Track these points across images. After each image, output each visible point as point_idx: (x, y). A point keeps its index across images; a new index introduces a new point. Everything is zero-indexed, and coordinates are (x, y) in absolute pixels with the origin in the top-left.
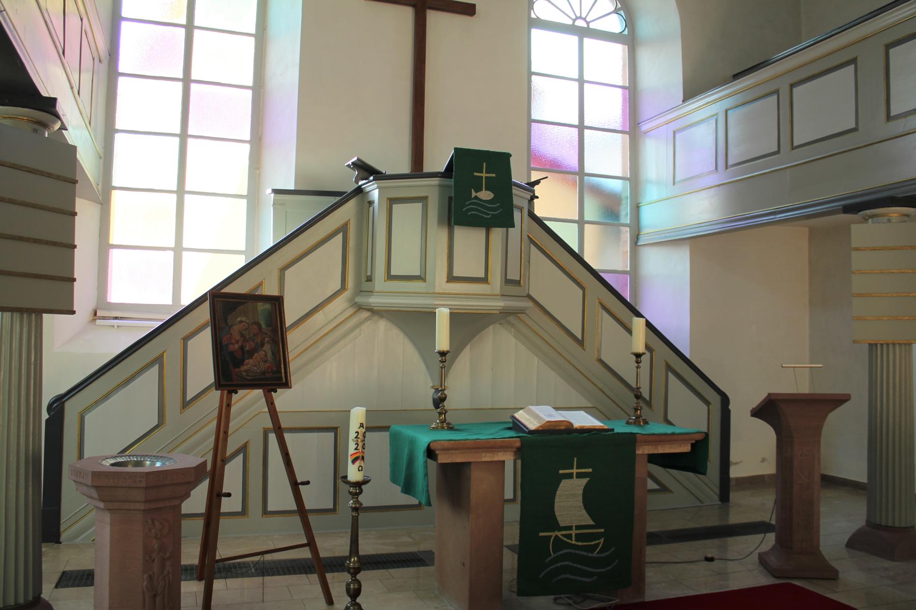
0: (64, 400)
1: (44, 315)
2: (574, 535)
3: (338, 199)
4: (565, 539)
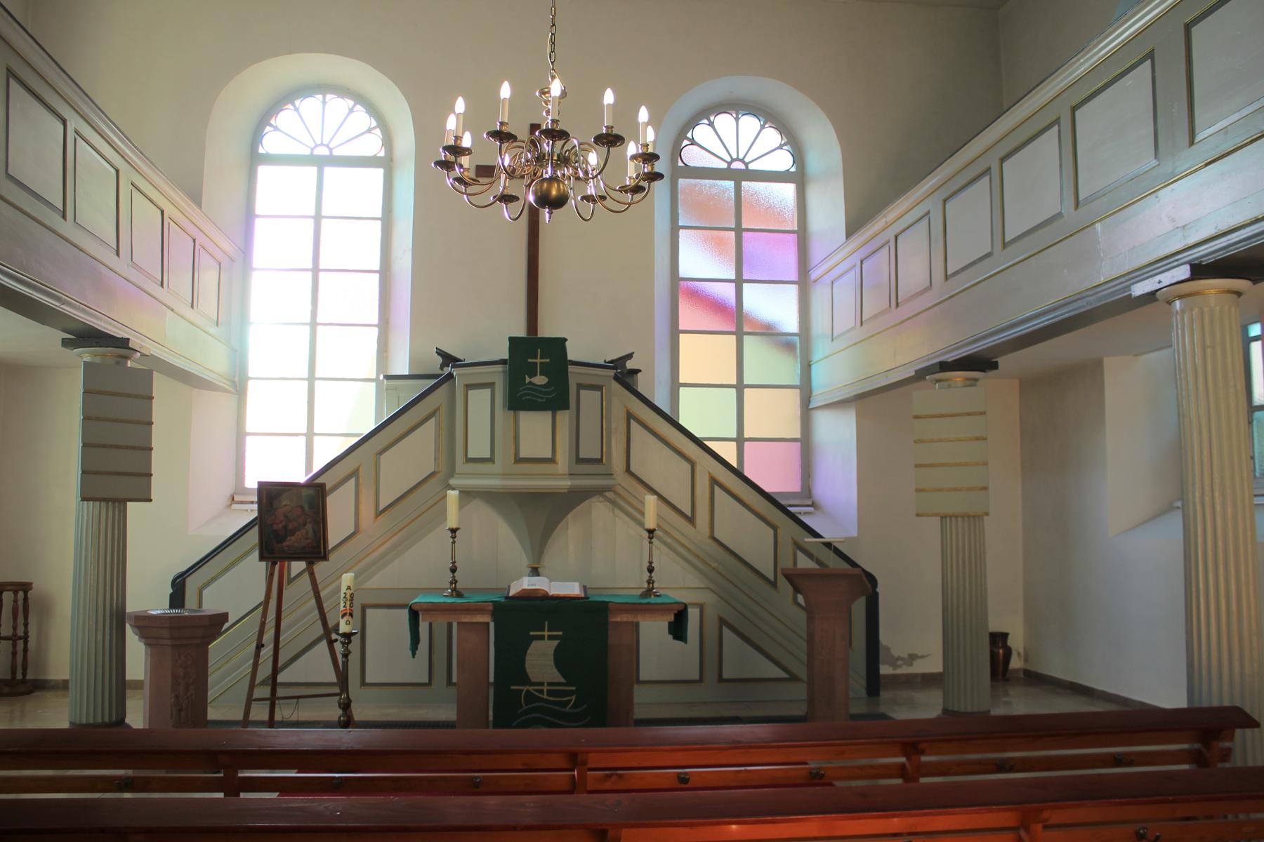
0: (185, 576)
1: (129, 503)
2: (545, 691)
4: (537, 694)
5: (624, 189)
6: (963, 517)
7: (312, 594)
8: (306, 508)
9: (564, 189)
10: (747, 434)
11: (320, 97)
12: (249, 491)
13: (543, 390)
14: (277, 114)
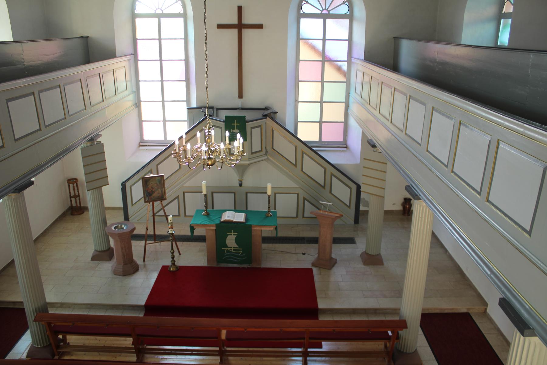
8: (158, 183)
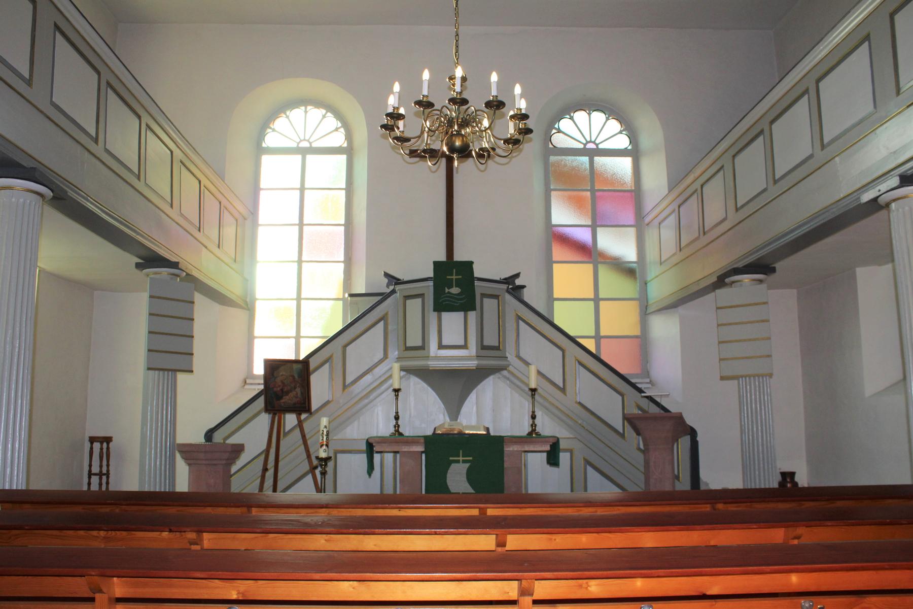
3: (380, 298)
5: (507, 141)
6: (754, 376)
7: (301, 441)
9: (466, 141)
10: (602, 333)
11: (303, 108)
12: (258, 377)
13: (458, 297)
14: (274, 120)
